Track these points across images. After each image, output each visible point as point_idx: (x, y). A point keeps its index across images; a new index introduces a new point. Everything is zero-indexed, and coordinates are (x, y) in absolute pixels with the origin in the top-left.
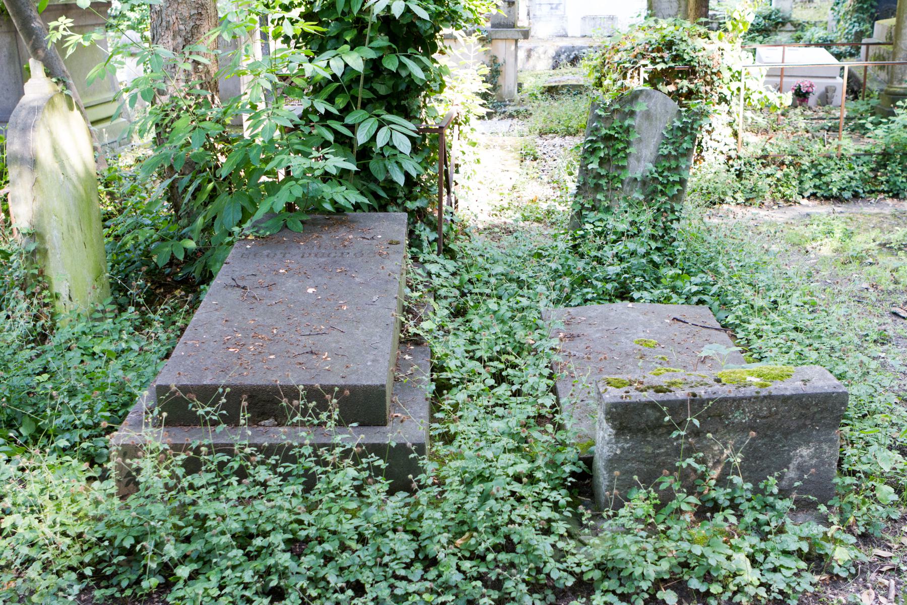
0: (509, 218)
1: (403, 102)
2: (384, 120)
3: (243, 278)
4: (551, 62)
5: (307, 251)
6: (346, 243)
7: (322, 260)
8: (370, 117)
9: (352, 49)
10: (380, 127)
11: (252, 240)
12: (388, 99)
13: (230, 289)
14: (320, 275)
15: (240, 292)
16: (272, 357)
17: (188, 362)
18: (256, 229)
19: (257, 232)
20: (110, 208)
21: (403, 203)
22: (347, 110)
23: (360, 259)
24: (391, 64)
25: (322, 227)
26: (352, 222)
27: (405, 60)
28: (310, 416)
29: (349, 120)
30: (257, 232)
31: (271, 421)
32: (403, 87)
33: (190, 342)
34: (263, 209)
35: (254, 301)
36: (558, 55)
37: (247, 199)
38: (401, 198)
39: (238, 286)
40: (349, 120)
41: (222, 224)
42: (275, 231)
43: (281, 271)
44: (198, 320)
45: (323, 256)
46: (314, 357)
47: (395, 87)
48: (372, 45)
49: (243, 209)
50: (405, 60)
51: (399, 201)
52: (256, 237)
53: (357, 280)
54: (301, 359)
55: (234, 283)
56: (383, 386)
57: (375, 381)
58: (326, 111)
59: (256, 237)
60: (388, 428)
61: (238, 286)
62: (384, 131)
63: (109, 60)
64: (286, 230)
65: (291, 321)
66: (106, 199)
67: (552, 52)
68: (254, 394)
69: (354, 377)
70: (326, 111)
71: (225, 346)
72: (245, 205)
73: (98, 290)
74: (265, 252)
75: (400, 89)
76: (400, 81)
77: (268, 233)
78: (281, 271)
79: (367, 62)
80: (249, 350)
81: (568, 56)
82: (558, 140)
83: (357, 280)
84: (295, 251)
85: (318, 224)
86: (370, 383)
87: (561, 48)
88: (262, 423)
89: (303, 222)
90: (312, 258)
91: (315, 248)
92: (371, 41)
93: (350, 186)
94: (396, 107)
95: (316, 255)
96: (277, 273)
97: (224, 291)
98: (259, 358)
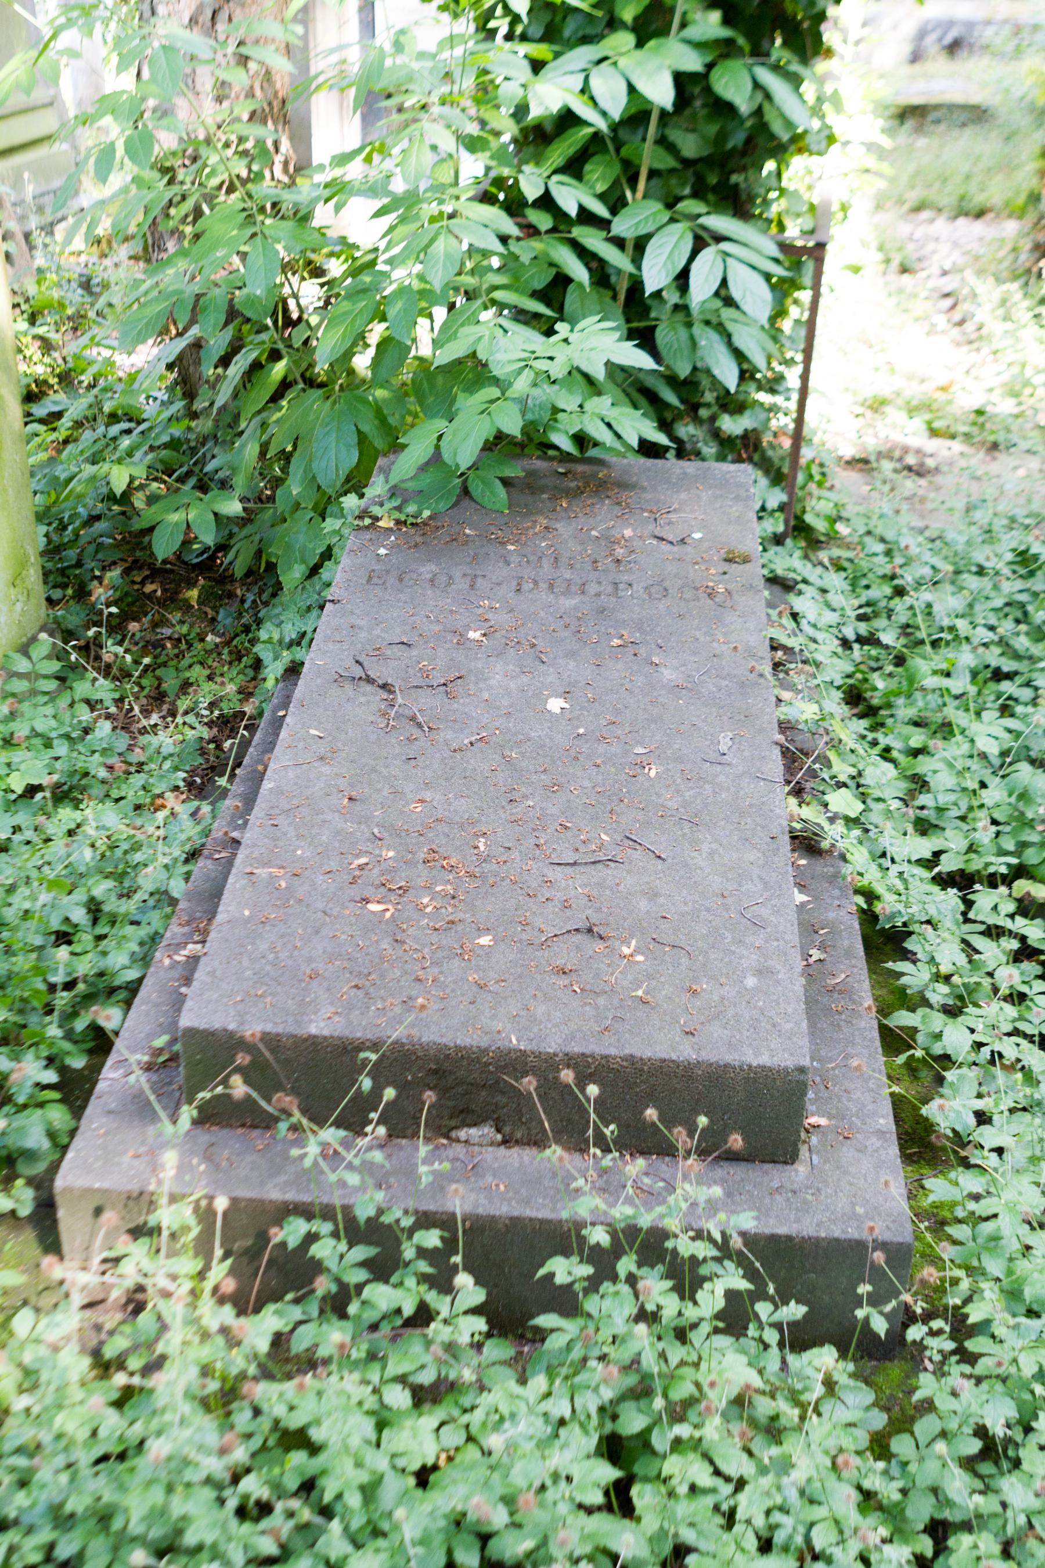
0: (908, 432)
1: (734, 178)
2: (704, 228)
3: (378, 653)
4: (906, 49)
5: (528, 572)
6: (620, 552)
7: (569, 603)
8: (673, 220)
9: (640, 44)
10: (699, 245)
11: (389, 530)
12: (699, 167)
13: (349, 687)
14: (572, 654)
15: (376, 697)
16: (485, 940)
17: (263, 946)
18: (396, 503)
19: (399, 509)
20: (40, 370)
21: (713, 418)
22: (616, 204)
23: (662, 606)
24: (733, 85)
25: (554, 498)
26: (623, 485)
27: (765, 76)
28: (629, 1201)
29: (624, 226)
30: (399, 509)
31: (486, 1131)
32: (737, 139)
33: (262, 872)
34: (418, 448)
35: (416, 732)
36: (922, 34)
37: (371, 415)
38: (708, 405)
39: (370, 680)
40: (624, 226)
41: (308, 469)
42: (442, 506)
43: (472, 635)
44: (278, 791)
45: (567, 593)
46: (599, 946)
47: (722, 137)
48: (688, 33)
49: (362, 439)
50: (765, 76)
51: (704, 413)
52: (398, 522)
53: (668, 675)
54: (564, 954)
55: (358, 672)
56: (802, 1070)
57: (789, 1062)
58: (582, 209)
59: (398, 522)
60: (801, 1169)
61: (370, 680)
62: (708, 255)
63: (46, 46)
64: (466, 502)
65: (518, 810)
66: (33, 350)
67: (909, 28)
68: (446, 1065)
69: (716, 1031)
70: (582, 209)
71: (355, 892)
72: (365, 428)
73: (19, 606)
74: (427, 570)
75: (730, 145)
76: (731, 125)
77: (426, 514)
78: (472, 635)
79: (681, 80)
80: (420, 909)
81: (940, 40)
82: (941, 226)
83: (668, 675)
84: (496, 571)
85: (542, 489)
86: (764, 1059)
87: (928, 22)
88: (462, 1134)
89: (506, 482)
90: (543, 595)
91: (546, 564)
92: (683, 25)
93: (651, 413)
94: (714, 189)
95: (551, 587)
96: (462, 641)
97: (334, 691)
98: (448, 940)
